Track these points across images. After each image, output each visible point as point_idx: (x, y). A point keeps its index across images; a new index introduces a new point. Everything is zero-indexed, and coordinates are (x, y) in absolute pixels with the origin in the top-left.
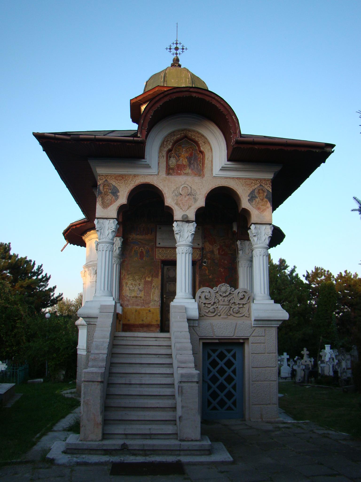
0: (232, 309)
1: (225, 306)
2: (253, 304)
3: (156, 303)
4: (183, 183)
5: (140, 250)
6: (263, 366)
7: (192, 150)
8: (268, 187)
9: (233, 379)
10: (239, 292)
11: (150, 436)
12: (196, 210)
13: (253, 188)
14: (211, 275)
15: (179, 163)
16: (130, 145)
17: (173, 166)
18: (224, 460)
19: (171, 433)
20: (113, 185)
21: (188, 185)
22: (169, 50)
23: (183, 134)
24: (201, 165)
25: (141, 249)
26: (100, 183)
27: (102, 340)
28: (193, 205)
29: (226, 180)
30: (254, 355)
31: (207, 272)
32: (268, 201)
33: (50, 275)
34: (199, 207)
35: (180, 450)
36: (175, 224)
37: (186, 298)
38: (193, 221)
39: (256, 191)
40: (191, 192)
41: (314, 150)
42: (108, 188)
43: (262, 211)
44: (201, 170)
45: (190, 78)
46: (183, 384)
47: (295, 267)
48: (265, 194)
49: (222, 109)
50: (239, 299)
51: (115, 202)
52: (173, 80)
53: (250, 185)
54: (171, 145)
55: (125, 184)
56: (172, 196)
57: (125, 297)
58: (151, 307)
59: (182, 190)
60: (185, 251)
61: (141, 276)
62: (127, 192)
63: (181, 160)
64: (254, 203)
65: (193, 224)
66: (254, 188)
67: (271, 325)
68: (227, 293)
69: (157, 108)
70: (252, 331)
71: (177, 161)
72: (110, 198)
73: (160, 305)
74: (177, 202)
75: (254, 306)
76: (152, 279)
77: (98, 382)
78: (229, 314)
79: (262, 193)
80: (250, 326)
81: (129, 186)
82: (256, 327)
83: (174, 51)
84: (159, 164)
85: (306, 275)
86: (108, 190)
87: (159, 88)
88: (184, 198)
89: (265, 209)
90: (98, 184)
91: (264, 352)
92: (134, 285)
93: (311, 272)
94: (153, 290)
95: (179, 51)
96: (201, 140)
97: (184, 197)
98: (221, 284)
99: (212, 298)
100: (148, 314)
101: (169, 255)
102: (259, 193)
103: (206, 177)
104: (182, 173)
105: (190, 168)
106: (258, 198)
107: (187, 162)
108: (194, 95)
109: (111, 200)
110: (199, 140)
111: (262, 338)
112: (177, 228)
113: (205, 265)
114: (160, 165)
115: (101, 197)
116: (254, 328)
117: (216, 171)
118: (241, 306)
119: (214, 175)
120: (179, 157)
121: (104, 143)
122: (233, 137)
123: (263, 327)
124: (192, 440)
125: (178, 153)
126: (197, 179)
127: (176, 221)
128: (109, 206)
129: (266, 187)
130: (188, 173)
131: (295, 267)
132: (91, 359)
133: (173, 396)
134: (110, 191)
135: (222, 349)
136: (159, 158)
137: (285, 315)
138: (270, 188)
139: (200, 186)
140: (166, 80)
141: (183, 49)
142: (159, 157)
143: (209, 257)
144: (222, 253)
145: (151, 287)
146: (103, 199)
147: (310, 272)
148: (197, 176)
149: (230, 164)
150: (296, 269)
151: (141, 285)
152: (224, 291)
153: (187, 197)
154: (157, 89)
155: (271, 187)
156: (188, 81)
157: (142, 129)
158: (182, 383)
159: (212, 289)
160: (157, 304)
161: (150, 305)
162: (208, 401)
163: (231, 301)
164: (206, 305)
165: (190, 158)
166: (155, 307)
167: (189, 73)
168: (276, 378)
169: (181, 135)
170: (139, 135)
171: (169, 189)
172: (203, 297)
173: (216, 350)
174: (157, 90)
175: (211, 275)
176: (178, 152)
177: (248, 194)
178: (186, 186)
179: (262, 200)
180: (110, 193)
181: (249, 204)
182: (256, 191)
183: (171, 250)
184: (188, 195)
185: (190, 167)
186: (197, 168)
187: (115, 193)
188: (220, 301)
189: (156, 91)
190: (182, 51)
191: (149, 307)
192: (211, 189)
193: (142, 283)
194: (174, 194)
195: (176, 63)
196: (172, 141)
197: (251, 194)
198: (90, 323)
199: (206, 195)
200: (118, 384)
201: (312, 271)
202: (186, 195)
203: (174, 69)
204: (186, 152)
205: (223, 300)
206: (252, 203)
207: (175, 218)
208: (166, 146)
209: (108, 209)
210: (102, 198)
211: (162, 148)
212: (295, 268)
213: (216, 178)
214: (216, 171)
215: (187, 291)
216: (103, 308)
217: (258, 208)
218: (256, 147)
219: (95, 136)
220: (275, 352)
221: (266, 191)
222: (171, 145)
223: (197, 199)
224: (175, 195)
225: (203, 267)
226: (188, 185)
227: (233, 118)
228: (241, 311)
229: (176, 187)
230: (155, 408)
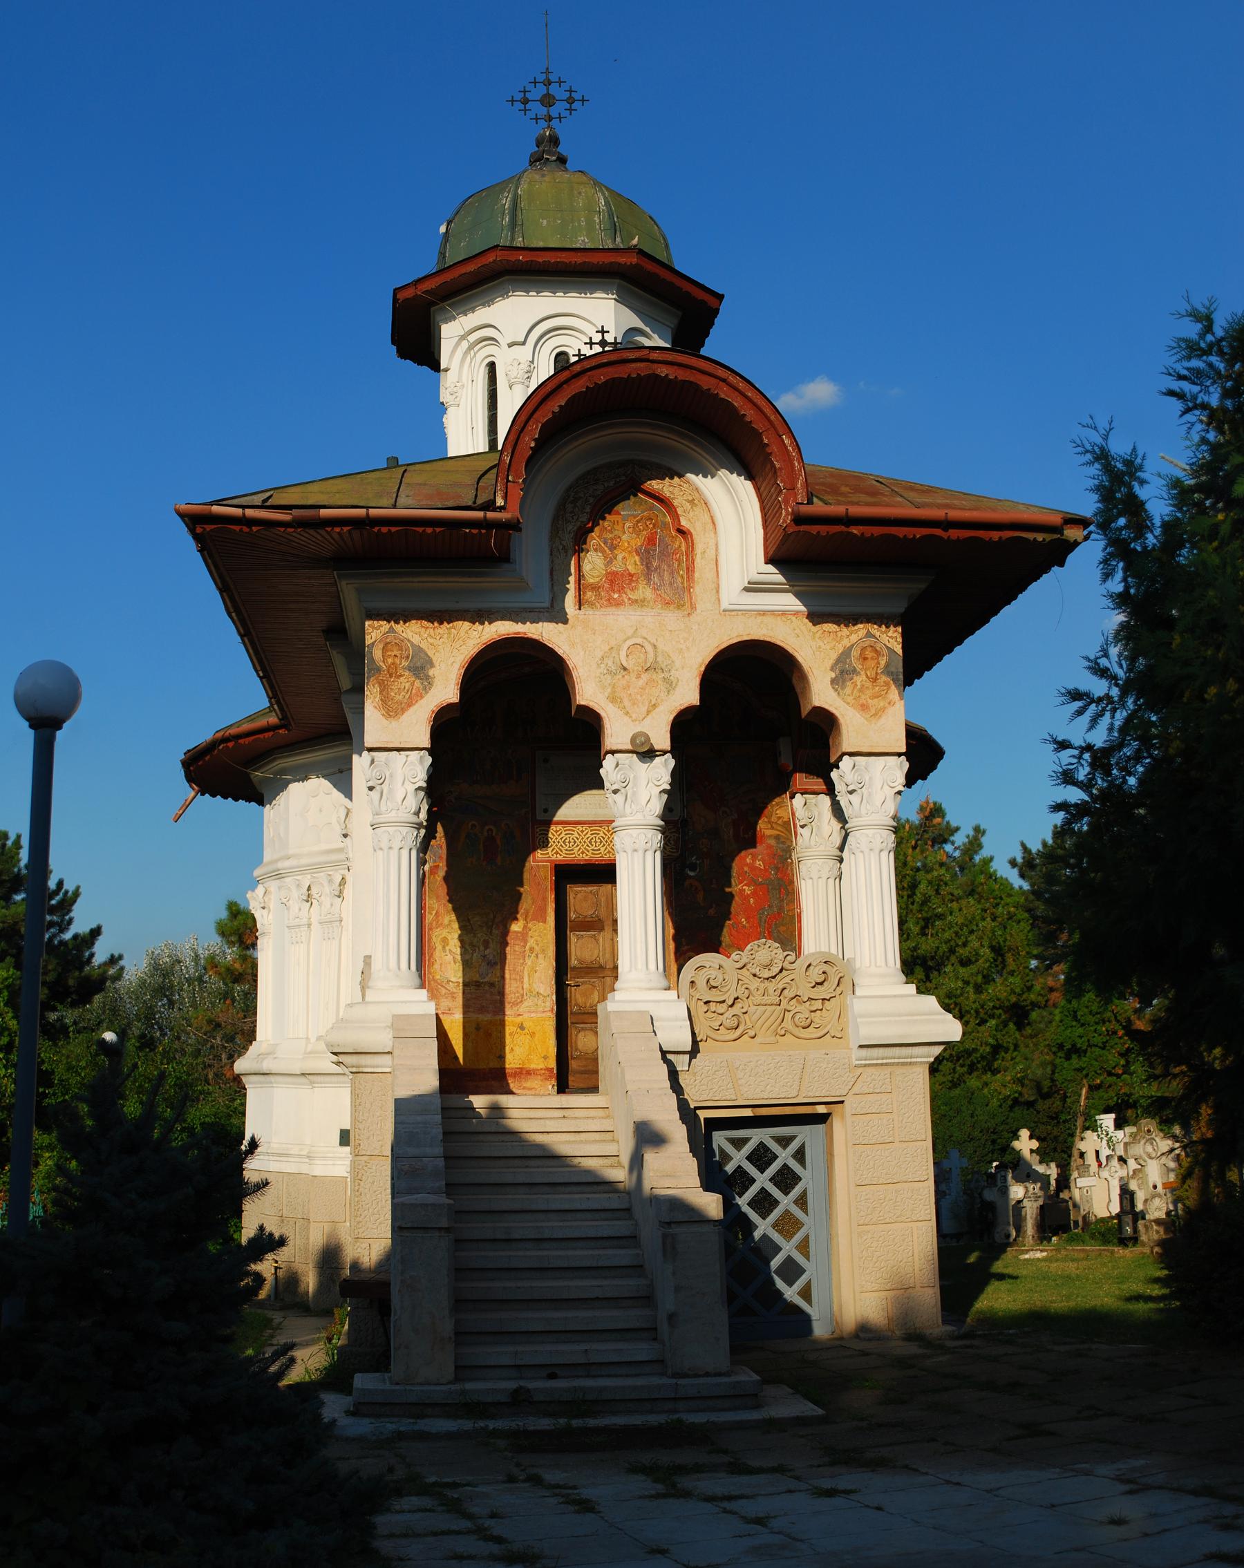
0: (792, 1013)
1: (770, 1008)
2: (855, 1000)
3: (540, 1002)
4: (630, 634)
5: (486, 834)
6: (889, 1181)
7: (654, 525)
8: (890, 640)
9: (798, 1225)
10: (809, 965)
11: (588, 1368)
12: (672, 718)
13: (847, 643)
14: (714, 906)
15: (614, 569)
16: (475, 531)
17: (597, 579)
18: (799, 1415)
19: (647, 1359)
20: (412, 644)
21: (645, 638)
22: (522, 107)
23: (623, 478)
24: (681, 572)
25: (487, 828)
26: (373, 640)
27: (419, 1118)
28: (662, 700)
29: (759, 619)
30: (861, 1148)
31: (700, 896)
32: (892, 682)
33: (78, 888)
34: (682, 708)
35: (675, 1399)
36: (608, 763)
37: (650, 989)
38: (665, 753)
39: (855, 653)
40: (656, 662)
41: (1030, 536)
42: (398, 653)
43: (875, 715)
44: (684, 587)
45: (603, 210)
46: (675, 1230)
47: (977, 830)
48: (883, 662)
49: (749, 414)
50: (813, 985)
51: (422, 697)
52: (545, 222)
53: (837, 636)
54: (587, 513)
55: (451, 639)
56: (598, 675)
57: (442, 986)
58: (526, 1015)
59: (627, 656)
60: (641, 844)
61: (492, 916)
62: (457, 666)
63: (620, 557)
64: (848, 690)
65: (666, 760)
66: (849, 645)
67: (909, 1060)
68: (775, 970)
69: (550, 416)
70: (854, 1080)
71: (609, 562)
72: (407, 685)
73: (555, 1008)
74: (613, 692)
75: (857, 1006)
76: (525, 927)
77: (440, 1229)
78: (783, 1032)
79: (872, 658)
80: (847, 1066)
81: (464, 647)
82: (865, 1065)
83: (537, 109)
84: (554, 573)
85: (1019, 860)
86: (398, 661)
87: (499, 253)
88: (634, 679)
89: (883, 709)
90: (368, 641)
91: (891, 1139)
92: (468, 947)
93: (1040, 847)
94: (529, 962)
95: (559, 108)
96: (682, 493)
97: (633, 676)
98: (756, 942)
99: (729, 986)
100: (516, 1036)
101: (578, 846)
102: (865, 659)
103: (698, 611)
104: (626, 600)
105: (648, 584)
106: (862, 673)
107: (639, 563)
108: (663, 371)
109: (408, 691)
110: (674, 494)
111: (885, 1096)
112: (617, 774)
113: (692, 874)
114: (555, 577)
115: (379, 683)
116: (860, 1070)
117: (732, 592)
118: (818, 1005)
119: (725, 604)
120: (613, 548)
121: (393, 529)
122: (786, 501)
123: (886, 1064)
124: (707, 1374)
125: (610, 536)
126: (672, 618)
127: (613, 752)
128: (403, 711)
129: (884, 639)
130: (643, 600)
131: (977, 830)
132: (402, 1170)
133: (637, 1269)
134: (405, 663)
135: (758, 1136)
136: (551, 555)
137: (951, 1029)
138: (896, 641)
139: (682, 641)
140: (519, 222)
141: (571, 101)
142: (551, 551)
143: (705, 850)
144: (746, 836)
145: (524, 951)
146: (384, 688)
147: (1035, 847)
148: (672, 607)
149: (774, 575)
150: (984, 840)
151: (491, 945)
152: (765, 963)
153: (642, 676)
154: (491, 258)
155: (900, 640)
156: (598, 221)
157: (508, 481)
158: (673, 1225)
159: (729, 957)
160: (543, 1004)
161: (521, 1010)
162: (805, 1211)
163: (786, 992)
164: (713, 1006)
165: (649, 553)
166: (539, 1015)
167: (600, 194)
168: (928, 1211)
169: (618, 480)
170: (500, 502)
171: (587, 653)
172: (701, 983)
173: (745, 1141)
174: (491, 260)
175: (714, 906)
176: (611, 532)
177: (832, 662)
178: (639, 641)
179: (875, 680)
180: (404, 668)
181: (834, 694)
182: (855, 653)
183: (582, 831)
184: (646, 670)
185: (649, 580)
186: (671, 584)
187: (421, 667)
188: (754, 992)
189: (490, 263)
190: (568, 106)
191: (519, 1015)
192: (717, 651)
193: (493, 940)
194: (603, 669)
195: (549, 153)
196: (591, 500)
197: (838, 661)
198: (361, 1070)
199: (703, 669)
200: (471, 1240)
201: (1044, 844)
202: (640, 669)
203: (545, 181)
204: (636, 531)
205: (762, 991)
206: (843, 689)
207: (610, 741)
208: (572, 517)
209: (401, 720)
210: (380, 686)
211: (560, 522)
212: (980, 835)
213: (730, 613)
214: (732, 592)
215: (652, 966)
216: (401, 1026)
217: (862, 705)
218: (855, 532)
219: (368, 508)
220: (924, 1137)
221: (885, 652)
222: (587, 513)
223: (674, 683)
224: (605, 671)
225: (687, 883)
226: (645, 638)
227: (783, 441)
228: (817, 1020)
229: (609, 647)
230: (591, 1299)
